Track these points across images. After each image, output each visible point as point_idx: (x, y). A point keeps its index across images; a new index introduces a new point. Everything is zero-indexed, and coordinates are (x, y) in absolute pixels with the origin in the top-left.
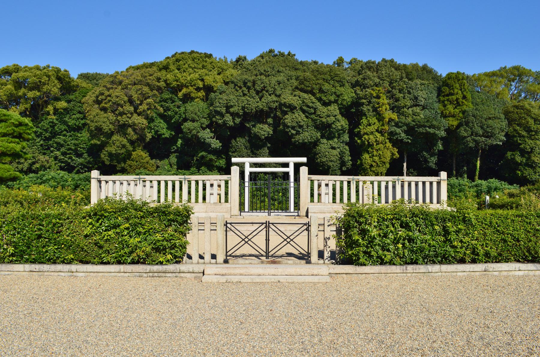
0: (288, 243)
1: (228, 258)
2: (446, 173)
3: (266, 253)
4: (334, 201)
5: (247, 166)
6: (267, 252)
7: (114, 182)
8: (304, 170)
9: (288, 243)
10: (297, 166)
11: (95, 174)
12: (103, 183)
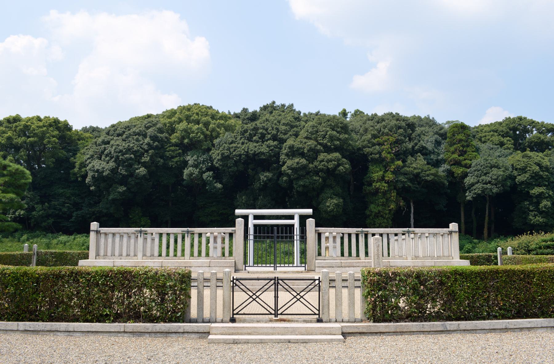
0: (298, 300)
1: (235, 316)
2: (92, 223)
3: (275, 311)
4: (342, 255)
5: (251, 218)
6: (276, 310)
7: (121, 236)
8: (311, 222)
9: (298, 300)
10: (303, 219)
11: (94, 225)
12: (370, 236)
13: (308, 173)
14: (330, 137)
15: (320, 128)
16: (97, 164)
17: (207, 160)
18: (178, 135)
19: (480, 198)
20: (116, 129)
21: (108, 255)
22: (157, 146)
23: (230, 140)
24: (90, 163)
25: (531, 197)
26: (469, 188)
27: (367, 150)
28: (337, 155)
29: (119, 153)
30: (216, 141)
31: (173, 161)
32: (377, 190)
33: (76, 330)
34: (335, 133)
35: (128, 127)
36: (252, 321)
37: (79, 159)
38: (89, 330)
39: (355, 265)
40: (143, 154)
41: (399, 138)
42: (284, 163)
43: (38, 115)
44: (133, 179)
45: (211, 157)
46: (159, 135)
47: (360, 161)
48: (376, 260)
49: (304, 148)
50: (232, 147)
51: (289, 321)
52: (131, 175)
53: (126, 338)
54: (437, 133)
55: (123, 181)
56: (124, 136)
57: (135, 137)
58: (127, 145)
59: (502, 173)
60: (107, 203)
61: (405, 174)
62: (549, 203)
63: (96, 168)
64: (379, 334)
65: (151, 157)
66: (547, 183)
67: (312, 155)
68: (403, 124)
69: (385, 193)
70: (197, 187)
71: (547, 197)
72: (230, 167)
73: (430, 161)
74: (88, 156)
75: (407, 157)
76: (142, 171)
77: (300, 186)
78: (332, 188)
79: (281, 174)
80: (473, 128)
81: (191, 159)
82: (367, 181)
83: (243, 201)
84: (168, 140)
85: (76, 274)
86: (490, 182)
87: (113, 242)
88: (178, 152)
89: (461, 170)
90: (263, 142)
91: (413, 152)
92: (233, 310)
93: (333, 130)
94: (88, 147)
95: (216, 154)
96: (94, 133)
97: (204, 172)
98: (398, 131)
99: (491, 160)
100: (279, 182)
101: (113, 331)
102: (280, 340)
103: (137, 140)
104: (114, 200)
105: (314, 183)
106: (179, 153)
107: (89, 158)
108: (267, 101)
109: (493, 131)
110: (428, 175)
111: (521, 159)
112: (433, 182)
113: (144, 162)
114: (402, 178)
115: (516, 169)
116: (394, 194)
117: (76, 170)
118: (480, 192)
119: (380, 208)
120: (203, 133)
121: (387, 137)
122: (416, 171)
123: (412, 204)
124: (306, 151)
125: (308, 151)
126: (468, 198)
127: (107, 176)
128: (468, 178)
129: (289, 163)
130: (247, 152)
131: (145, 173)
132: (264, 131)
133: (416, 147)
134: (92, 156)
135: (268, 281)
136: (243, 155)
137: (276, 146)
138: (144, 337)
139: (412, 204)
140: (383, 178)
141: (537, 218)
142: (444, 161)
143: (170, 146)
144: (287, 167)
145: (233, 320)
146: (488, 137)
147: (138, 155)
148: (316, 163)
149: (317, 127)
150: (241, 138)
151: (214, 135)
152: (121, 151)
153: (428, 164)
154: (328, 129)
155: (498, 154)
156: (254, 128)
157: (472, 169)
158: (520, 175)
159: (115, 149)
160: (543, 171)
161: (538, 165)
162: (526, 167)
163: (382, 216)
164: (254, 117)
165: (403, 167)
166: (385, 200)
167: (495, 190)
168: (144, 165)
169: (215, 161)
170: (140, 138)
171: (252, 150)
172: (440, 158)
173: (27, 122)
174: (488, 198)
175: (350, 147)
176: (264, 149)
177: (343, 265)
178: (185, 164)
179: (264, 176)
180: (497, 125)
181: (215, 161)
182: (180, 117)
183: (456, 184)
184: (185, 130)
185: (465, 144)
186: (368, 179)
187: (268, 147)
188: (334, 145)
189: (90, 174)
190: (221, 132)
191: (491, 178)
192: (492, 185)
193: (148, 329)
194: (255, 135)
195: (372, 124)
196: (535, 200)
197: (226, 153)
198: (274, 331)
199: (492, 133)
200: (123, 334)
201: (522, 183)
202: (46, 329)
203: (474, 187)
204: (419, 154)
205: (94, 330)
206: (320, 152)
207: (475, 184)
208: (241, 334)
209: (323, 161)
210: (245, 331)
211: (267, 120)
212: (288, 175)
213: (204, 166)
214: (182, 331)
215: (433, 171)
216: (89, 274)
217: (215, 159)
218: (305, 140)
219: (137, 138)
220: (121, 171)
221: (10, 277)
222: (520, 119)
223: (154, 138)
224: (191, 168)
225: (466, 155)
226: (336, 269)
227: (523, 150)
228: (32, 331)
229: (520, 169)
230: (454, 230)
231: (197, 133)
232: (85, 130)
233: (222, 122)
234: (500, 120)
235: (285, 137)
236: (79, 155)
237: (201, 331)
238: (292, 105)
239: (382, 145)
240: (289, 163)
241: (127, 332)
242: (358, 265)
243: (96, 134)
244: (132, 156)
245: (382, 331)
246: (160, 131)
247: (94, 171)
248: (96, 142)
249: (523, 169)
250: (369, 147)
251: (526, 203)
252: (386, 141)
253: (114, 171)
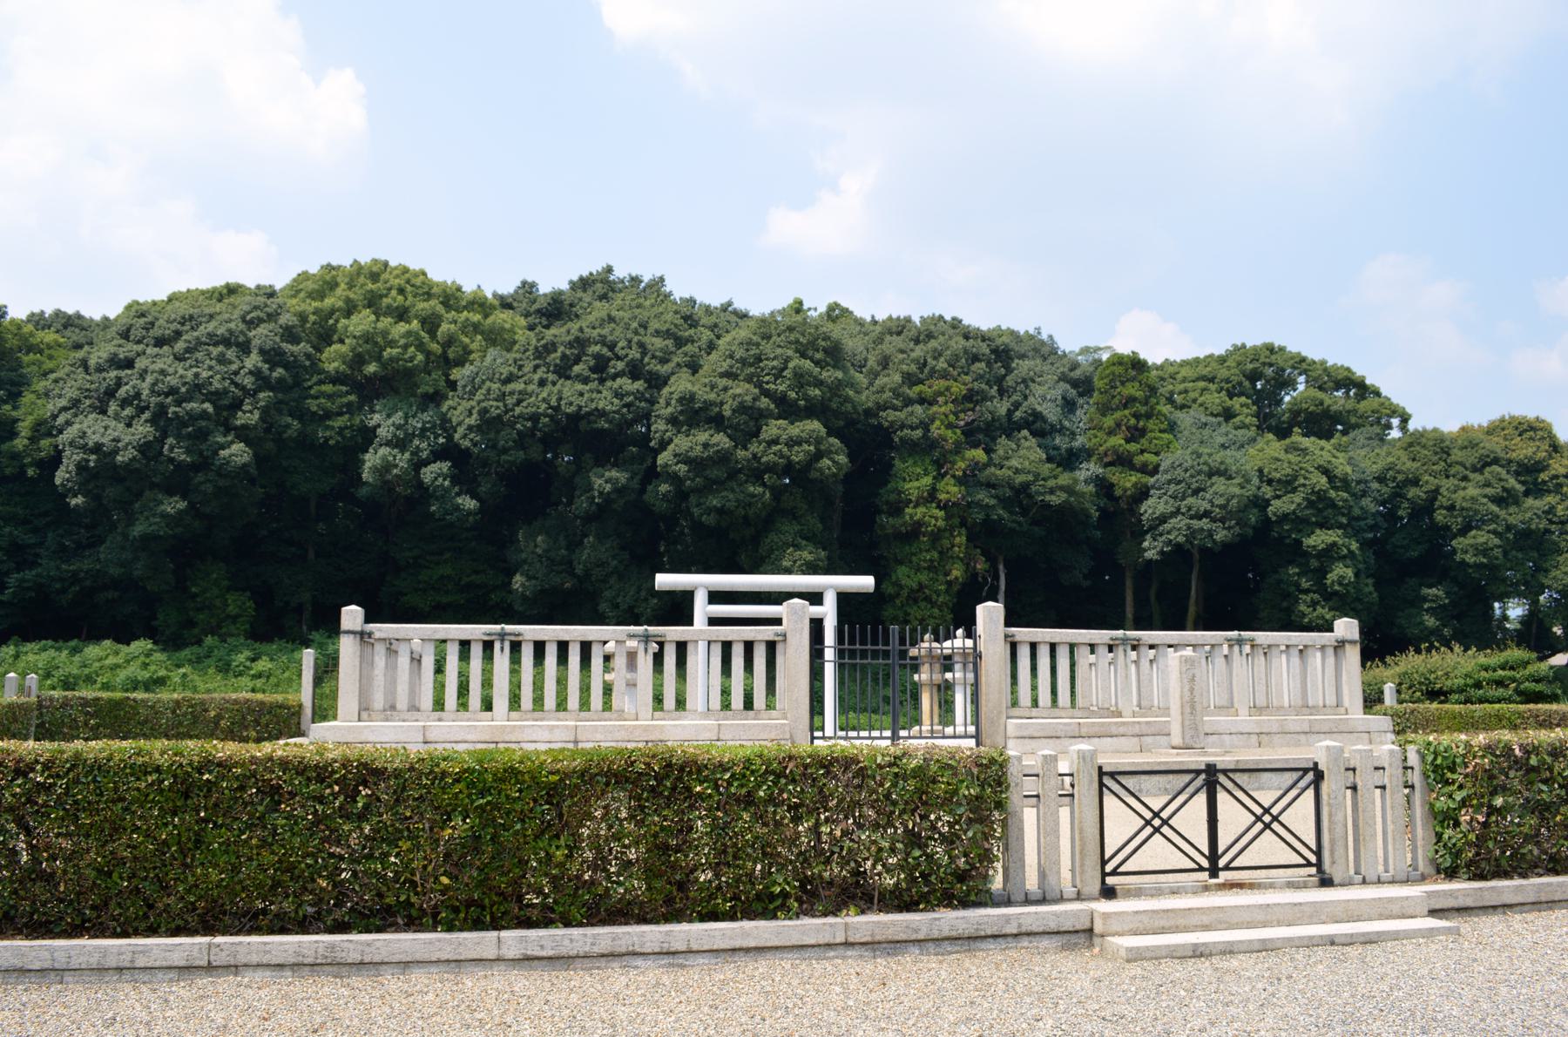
6: (1214, 856)
11: (352, 615)
13: (733, 474)
14: (796, 374)
15: (767, 347)
16: (96, 429)
17: (434, 426)
18: (343, 349)
19: (1178, 555)
20: (153, 324)
21: (399, 706)
22: (280, 380)
23: (505, 371)
24: (68, 423)
25: (1306, 554)
26: (1152, 528)
27: (891, 415)
28: (815, 426)
29: (167, 395)
30: (457, 374)
31: (328, 428)
32: (916, 529)
33: (695, 947)
34: (808, 364)
35: (191, 317)
36: (1158, 893)
37: (29, 410)
38: (737, 944)
39: (1114, 730)
40: (242, 402)
41: (976, 385)
42: (664, 445)
43: (325, 263)
44: (211, 476)
45: (445, 420)
46: (288, 347)
47: (872, 444)
48: (1187, 716)
49: (722, 403)
50: (512, 393)
51: (1252, 886)
52: (204, 463)
54: (1063, 378)
55: (178, 481)
56: (180, 346)
57: (215, 351)
58: (190, 374)
59: (1237, 491)
60: (123, 548)
61: (990, 485)
62: (1350, 573)
63: (92, 439)
64: (1500, 910)
65: (265, 412)
66: (1344, 520)
67: (747, 424)
68: (984, 349)
69: (936, 536)
70: (405, 504)
71: (1344, 557)
72: (505, 451)
73: (1052, 453)
74: (63, 402)
75: (994, 439)
76: (237, 452)
77: (709, 511)
78: (795, 518)
79: (652, 474)
80: (1158, 368)
81: (384, 421)
82: (887, 503)
83: (539, 551)
84: (313, 364)
85: (682, 769)
86: (1206, 514)
87: (515, 671)
88: (345, 400)
89: (1134, 479)
90: (602, 381)
91: (1010, 427)
92: (1104, 862)
93: (803, 356)
94: (60, 374)
95: (461, 412)
96: (68, 333)
97: (426, 463)
98: (973, 368)
99: (1210, 455)
100: (646, 497)
101: (813, 942)
102: (1311, 938)
103: (222, 360)
104: (146, 539)
105: (750, 505)
106: (349, 405)
107: (65, 409)
108: (590, 266)
109: (1203, 378)
110: (1052, 491)
111: (1282, 456)
112: (1063, 509)
113: (245, 427)
114: (983, 496)
115: (1270, 482)
116: (961, 539)
117: (20, 443)
118: (1181, 539)
119: (923, 577)
120: (421, 347)
121: (943, 383)
122: (1020, 479)
123: (1001, 567)
124: (727, 413)
125: (734, 411)
126: (1150, 555)
127: (126, 466)
128: (1150, 501)
129: (681, 443)
130: (557, 409)
131: (246, 458)
132: (605, 351)
133: (1018, 414)
134: (75, 403)
135: (1188, 778)
136: (546, 415)
137: (639, 396)
139: (1001, 567)
140: (931, 496)
141: (1320, 610)
142: (1087, 454)
143: (321, 382)
144: (675, 455)
145: (1109, 893)
146: (1192, 395)
147: (227, 405)
148: (754, 447)
149: (758, 345)
150: (536, 367)
151: (451, 355)
152: (172, 391)
153: (1049, 460)
154: (790, 353)
155: (1221, 440)
156: (577, 339)
157: (1161, 477)
158: (1278, 497)
159: (154, 384)
160: (1336, 489)
161: (1326, 472)
162: (1295, 478)
163: (928, 599)
164: (556, 309)
165: (986, 466)
166: (936, 555)
167: (1221, 535)
168: (243, 434)
169: (461, 430)
170: (231, 354)
171: (571, 404)
172: (1076, 444)
174: (1197, 556)
175: (849, 407)
176: (605, 400)
177: (1084, 731)
178: (367, 437)
179: (606, 480)
180: (1214, 365)
181: (461, 430)
182: (352, 296)
183: (1120, 514)
184: (367, 338)
185: (1143, 409)
186: (893, 497)
187: (618, 394)
188: (807, 398)
189: (71, 459)
190: (474, 346)
191: (1211, 501)
192: (1214, 520)
193: (916, 931)
194: (577, 361)
195: (902, 346)
196: (1314, 563)
197: (495, 408)
198: (1315, 914)
199: (1202, 384)
200: (841, 951)
201: (1285, 517)
202: (596, 950)
203: (1167, 526)
204: (1025, 432)
205: (753, 944)
206: (767, 417)
207: (1170, 519)
208: (1186, 929)
209: (775, 442)
210: (1195, 920)
211: (611, 319)
212: (675, 479)
213: (424, 445)
214: (1015, 931)
215: (1064, 479)
216: (723, 767)
217: (459, 424)
218: (724, 382)
219: (222, 354)
220: (171, 449)
221: (461, 786)
222: (1270, 349)
223: (272, 356)
224: (384, 451)
225: (1143, 441)
226: (1066, 742)
227: (1282, 433)
228: (550, 958)
229: (1279, 481)
230: (1349, 637)
231: (406, 347)
232: (38, 320)
233: (476, 317)
234: (1219, 350)
235: (664, 369)
236: (27, 398)
237: (1068, 926)
238: (662, 279)
239: (931, 404)
240: (681, 443)
241: (852, 944)
242: (1122, 730)
243: (75, 335)
244: (208, 407)
245: (1508, 902)
246: (290, 335)
247: (84, 447)
248: (84, 364)
249: (1288, 483)
250: (895, 409)
251: (1293, 570)
252: (940, 394)
253: (147, 450)
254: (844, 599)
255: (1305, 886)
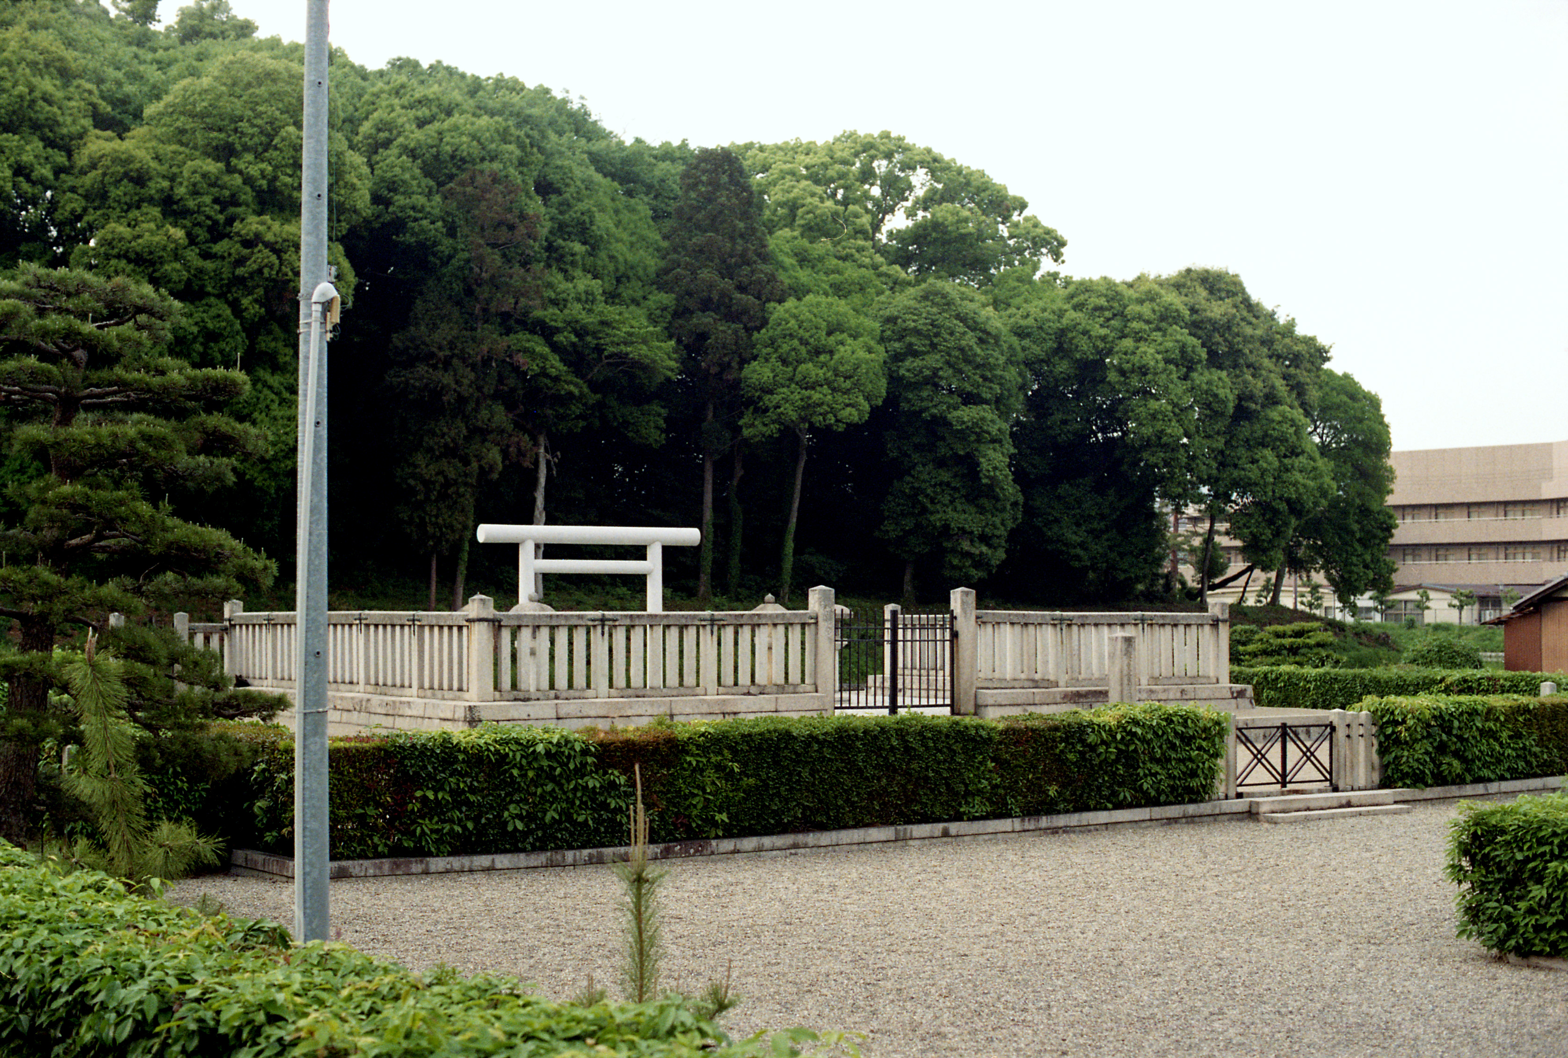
6: (1284, 775)
48: (1126, 687)
53: (1158, 832)
138: (409, 887)
173: (532, 105)
254: (670, 553)
255: (1326, 791)
